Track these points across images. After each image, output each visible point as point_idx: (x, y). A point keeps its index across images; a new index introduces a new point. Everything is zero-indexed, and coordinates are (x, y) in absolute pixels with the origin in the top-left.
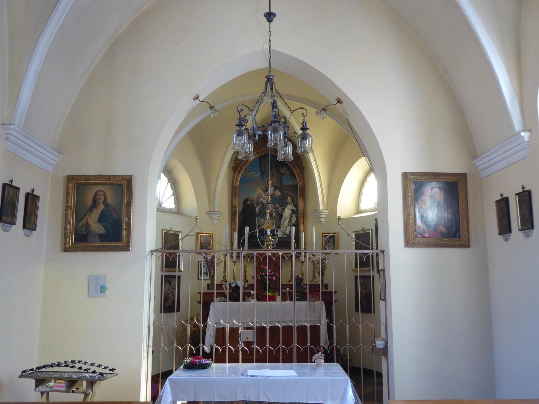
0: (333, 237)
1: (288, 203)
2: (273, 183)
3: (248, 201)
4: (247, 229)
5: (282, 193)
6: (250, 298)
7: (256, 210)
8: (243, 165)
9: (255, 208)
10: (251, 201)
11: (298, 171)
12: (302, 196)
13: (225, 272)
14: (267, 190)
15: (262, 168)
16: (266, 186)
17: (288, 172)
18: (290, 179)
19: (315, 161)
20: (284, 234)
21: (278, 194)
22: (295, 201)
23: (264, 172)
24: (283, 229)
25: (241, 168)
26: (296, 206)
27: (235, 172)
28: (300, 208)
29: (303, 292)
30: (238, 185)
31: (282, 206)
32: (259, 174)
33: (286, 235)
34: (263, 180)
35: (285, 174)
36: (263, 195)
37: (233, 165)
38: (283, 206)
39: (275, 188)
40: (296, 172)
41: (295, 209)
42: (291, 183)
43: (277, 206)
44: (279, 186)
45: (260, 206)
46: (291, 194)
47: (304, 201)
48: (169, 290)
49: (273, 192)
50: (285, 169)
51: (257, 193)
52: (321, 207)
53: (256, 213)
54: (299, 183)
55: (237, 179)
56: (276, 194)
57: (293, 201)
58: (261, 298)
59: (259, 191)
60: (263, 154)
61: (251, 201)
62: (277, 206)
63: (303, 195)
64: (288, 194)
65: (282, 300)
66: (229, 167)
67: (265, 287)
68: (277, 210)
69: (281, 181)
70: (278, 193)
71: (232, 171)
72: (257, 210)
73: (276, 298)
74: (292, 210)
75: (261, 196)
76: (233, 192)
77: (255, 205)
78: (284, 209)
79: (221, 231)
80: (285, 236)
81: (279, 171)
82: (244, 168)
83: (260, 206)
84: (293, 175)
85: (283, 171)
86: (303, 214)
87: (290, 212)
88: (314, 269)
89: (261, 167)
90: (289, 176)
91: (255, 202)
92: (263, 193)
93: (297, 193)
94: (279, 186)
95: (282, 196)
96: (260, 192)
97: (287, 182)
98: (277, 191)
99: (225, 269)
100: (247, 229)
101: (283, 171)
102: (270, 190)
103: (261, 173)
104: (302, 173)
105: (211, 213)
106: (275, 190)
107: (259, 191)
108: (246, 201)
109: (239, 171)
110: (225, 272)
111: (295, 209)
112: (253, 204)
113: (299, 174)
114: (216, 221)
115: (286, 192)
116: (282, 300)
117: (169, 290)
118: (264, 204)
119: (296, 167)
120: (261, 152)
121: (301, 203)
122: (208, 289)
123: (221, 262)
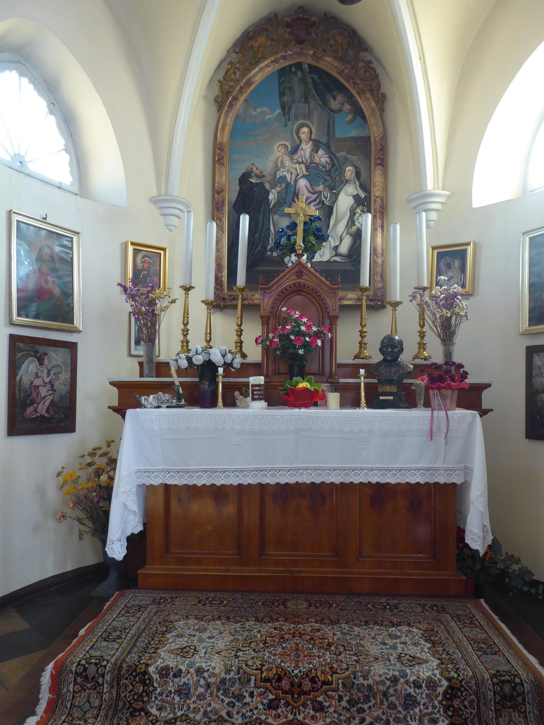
0: (461, 255)
1: (347, 181)
2: (311, 133)
3: (251, 177)
4: (245, 220)
5: (332, 155)
6: (249, 399)
7: (271, 197)
8: (241, 91)
9: (267, 193)
10: (257, 176)
11: (373, 104)
12: (382, 165)
13: (185, 332)
14: (295, 150)
15: (285, 98)
16: (293, 140)
17: (347, 107)
18: (351, 121)
19: (423, 58)
20: (336, 255)
21: (323, 160)
22: (363, 175)
23: (290, 108)
24: (332, 242)
25: (236, 99)
26: (365, 187)
27: (220, 109)
28: (376, 192)
29: (390, 383)
30: (226, 138)
31: (331, 188)
32: (279, 111)
33: (340, 255)
34: (286, 126)
35: (340, 111)
36: (288, 163)
37: (216, 91)
38: (335, 189)
39: (317, 145)
40: (366, 104)
41: (363, 195)
42: (354, 133)
43: (321, 188)
44: (324, 140)
45: (278, 189)
46: (354, 158)
47: (385, 174)
48: (37, 376)
49: (311, 155)
50: (339, 98)
51: (272, 158)
52: (430, 186)
53: (269, 204)
54: (375, 132)
55: (224, 125)
56: (317, 160)
57: (358, 175)
58: (278, 396)
59: (278, 152)
60: (288, 63)
61: (257, 176)
62: (321, 188)
63: (383, 162)
64: (346, 158)
65: (343, 405)
66: (205, 98)
67: (291, 373)
68: (319, 196)
69: (329, 128)
70: (322, 157)
71: (215, 108)
72: (272, 197)
73: (324, 397)
74: (356, 198)
75: (283, 166)
76: (218, 155)
77: (267, 186)
78: (337, 195)
79: (194, 248)
80: (337, 259)
81: (325, 104)
82: (242, 98)
83: (278, 189)
84: (358, 113)
85: (334, 105)
86: (382, 207)
87: (350, 201)
88: (422, 326)
89: (282, 94)
90: (350, 117)
91: (268, 178)
92: (286, 158)
93: (367, 155)
94: (324, 140)
95: (333, 165)
96: (280, 154)
97: (345, 129)
98: (321, 152)
99: (186, 324)
100: (245, 220)
101: (334, 105)
102: (306, 148)
103: (283, 108)
104: (382, 110)
105: (162, 201)
106: (315, 149)
107: (278, 152)
108: (244, 179)
109: (231, 106)
110: (185, 332)
111: (363, 195)
112: (262, 184)
113: (373, 110)
114: (174, 221)
115: (343, 153)
116: (343, 405)
117: (37, 376)
118: (288, 184)
119: (368, 95)
120: (284, 58)
121: (377, 178)
122: (141, 376)
123: (173, 302)
